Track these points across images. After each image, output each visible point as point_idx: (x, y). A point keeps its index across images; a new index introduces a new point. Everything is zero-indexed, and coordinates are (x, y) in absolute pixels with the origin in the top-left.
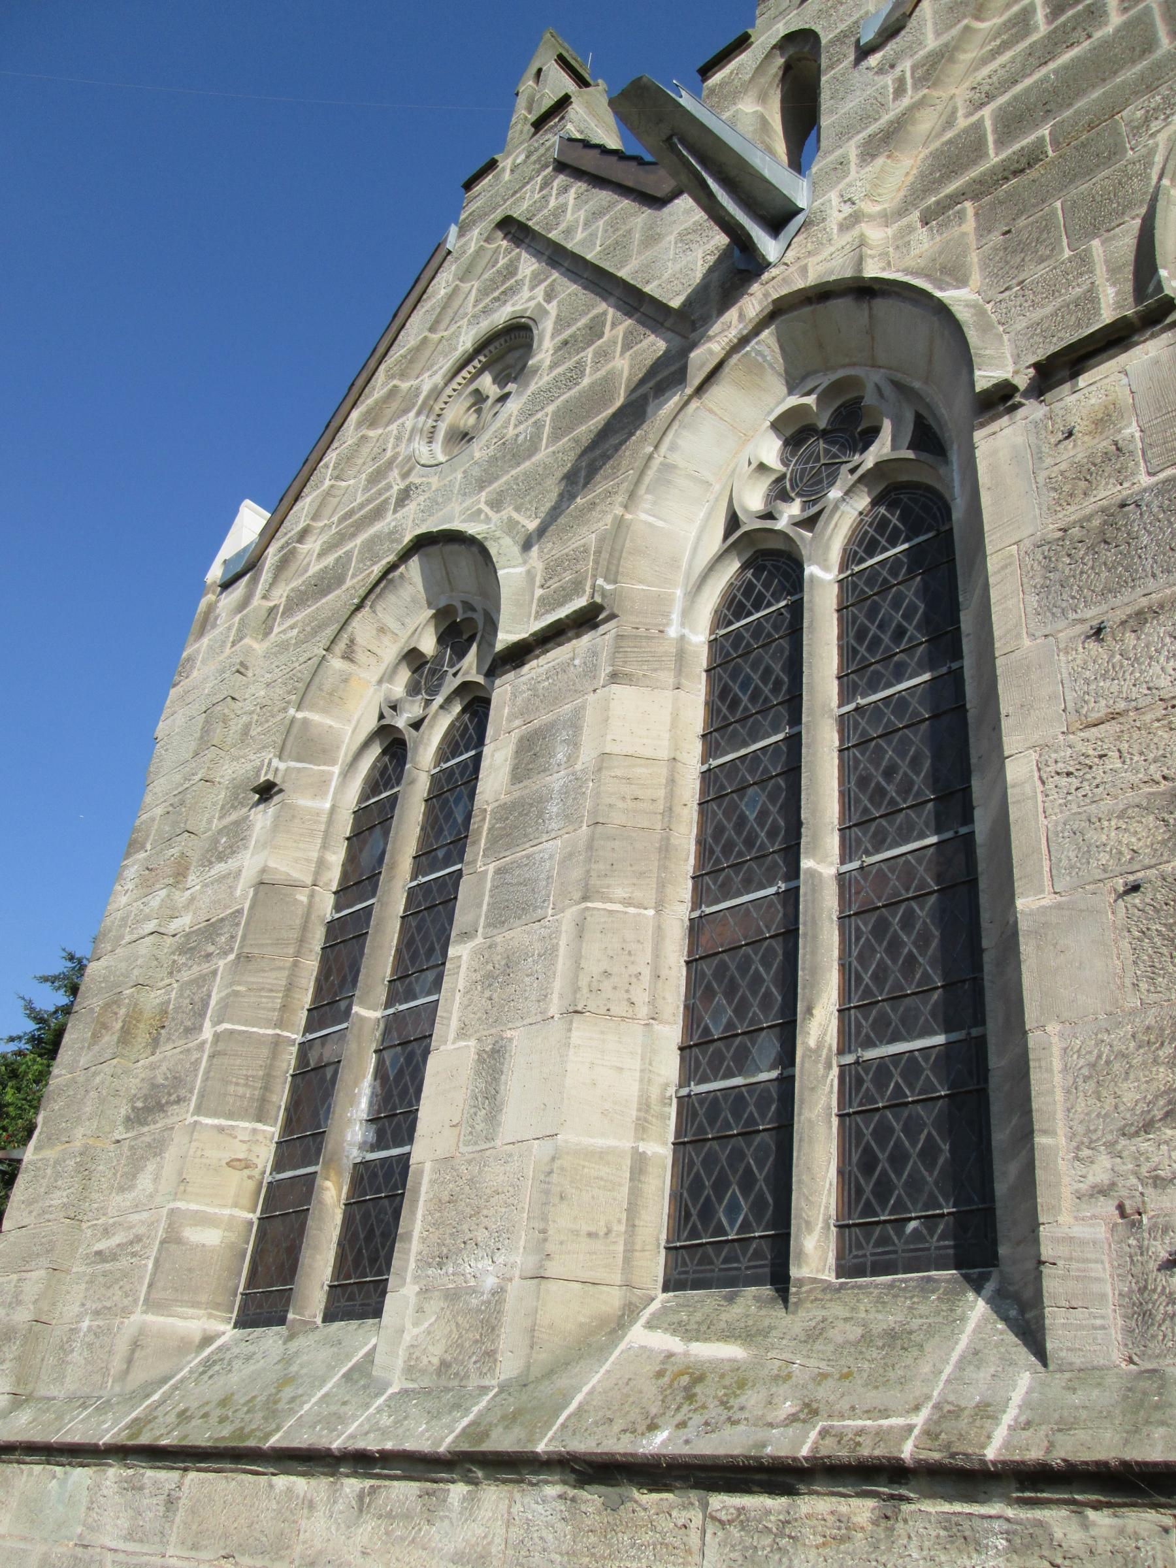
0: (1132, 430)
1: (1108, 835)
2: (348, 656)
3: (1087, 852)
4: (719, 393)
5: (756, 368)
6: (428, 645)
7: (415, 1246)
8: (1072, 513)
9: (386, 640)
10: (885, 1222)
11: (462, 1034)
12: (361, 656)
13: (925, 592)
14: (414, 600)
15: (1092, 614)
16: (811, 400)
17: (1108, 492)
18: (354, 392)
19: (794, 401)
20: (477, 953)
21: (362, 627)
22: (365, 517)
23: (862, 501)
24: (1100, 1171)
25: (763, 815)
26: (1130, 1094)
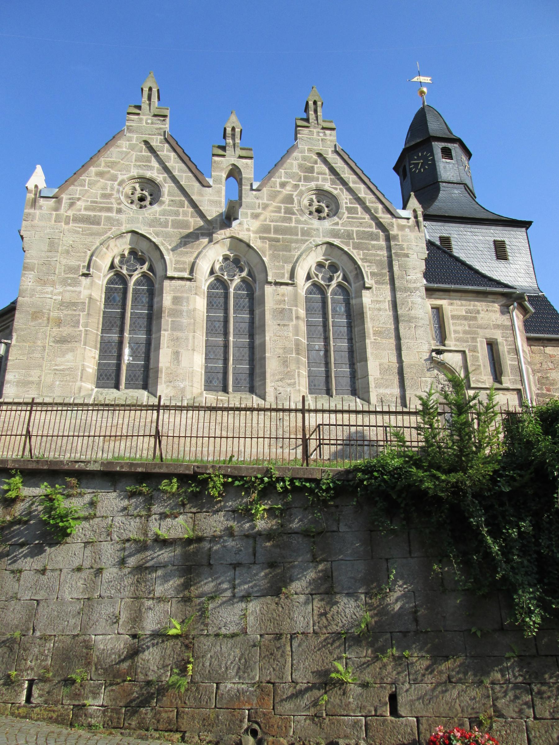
0: (286, 299)
1: (277, 350)
2: (107, 249)
3: (275, 351)
4: (217, 246)
5: (224, 244)
6: (126, 253)
7: (163, 379)
8: (277, 306)
9: (116, 248)
10: (120, 356)
11: (168, 347)
12: (110, 249)
13: (249, 301)
14: (126, 242)
15: (279, 322)
16: (232, 255)
17: (282, 306)
18: (92, 160)
19: (228, 253)
20: (169, 334)
21: (112, 243)
22: (103, 208)
23: (239, 280)
24: (273, 384)
25: (219, 327)
26: (277, 378)
